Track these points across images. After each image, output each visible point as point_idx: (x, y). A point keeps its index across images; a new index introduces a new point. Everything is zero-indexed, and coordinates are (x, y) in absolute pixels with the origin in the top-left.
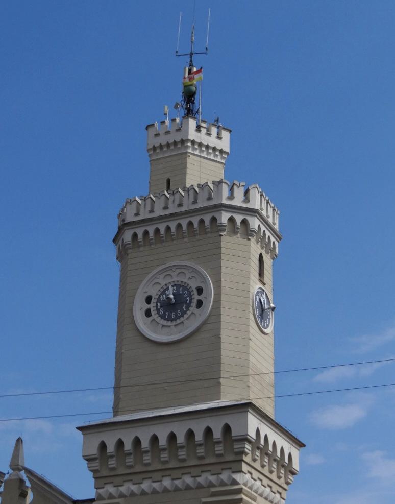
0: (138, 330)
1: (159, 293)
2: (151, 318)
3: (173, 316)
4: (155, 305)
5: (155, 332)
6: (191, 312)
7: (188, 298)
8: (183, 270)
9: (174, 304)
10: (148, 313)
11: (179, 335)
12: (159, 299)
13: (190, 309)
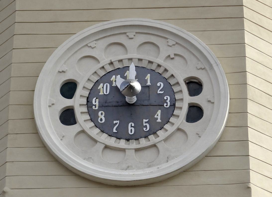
0: (44, 147)
1: (95, 78)
2: (74, 129)
3: (131, 130)
4: (84, 101)
5: (88, 159)
6: (175, 127)
7: (168, 98)
8: (186, 55)
9: (133, 105)
10: (68, 117)
11: (148, 170)
12: (93, 92)
13: (172, 119)
